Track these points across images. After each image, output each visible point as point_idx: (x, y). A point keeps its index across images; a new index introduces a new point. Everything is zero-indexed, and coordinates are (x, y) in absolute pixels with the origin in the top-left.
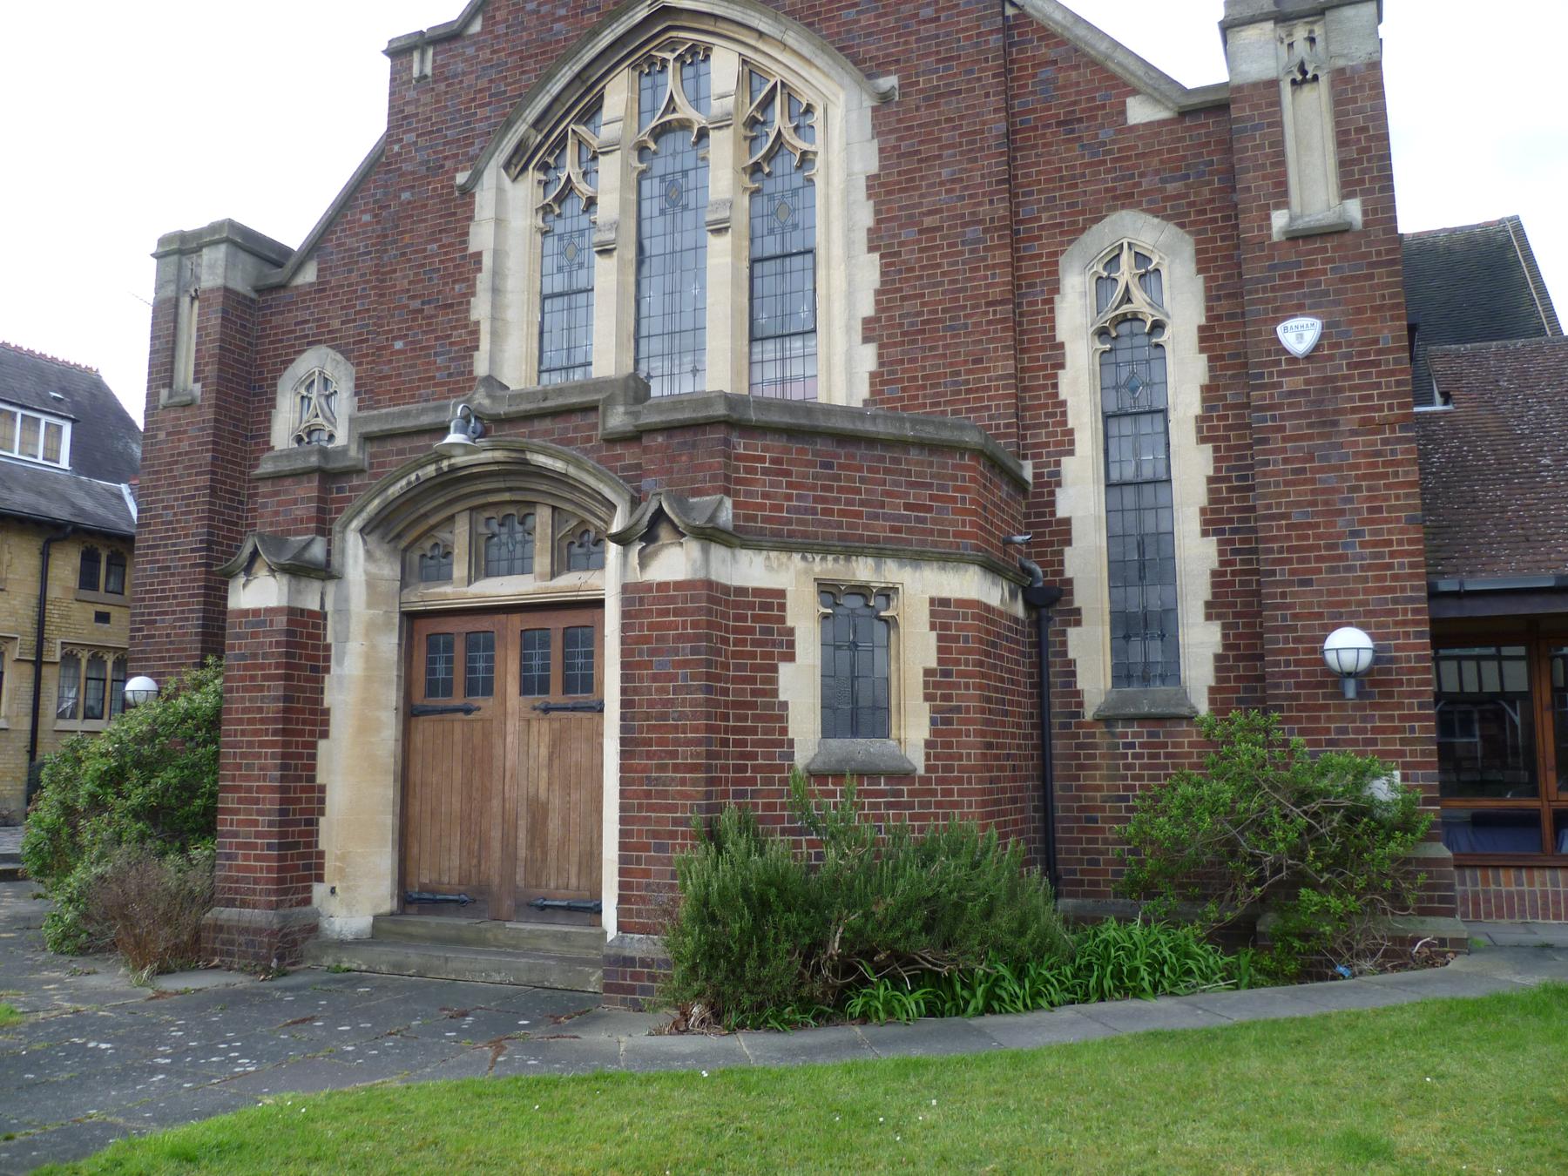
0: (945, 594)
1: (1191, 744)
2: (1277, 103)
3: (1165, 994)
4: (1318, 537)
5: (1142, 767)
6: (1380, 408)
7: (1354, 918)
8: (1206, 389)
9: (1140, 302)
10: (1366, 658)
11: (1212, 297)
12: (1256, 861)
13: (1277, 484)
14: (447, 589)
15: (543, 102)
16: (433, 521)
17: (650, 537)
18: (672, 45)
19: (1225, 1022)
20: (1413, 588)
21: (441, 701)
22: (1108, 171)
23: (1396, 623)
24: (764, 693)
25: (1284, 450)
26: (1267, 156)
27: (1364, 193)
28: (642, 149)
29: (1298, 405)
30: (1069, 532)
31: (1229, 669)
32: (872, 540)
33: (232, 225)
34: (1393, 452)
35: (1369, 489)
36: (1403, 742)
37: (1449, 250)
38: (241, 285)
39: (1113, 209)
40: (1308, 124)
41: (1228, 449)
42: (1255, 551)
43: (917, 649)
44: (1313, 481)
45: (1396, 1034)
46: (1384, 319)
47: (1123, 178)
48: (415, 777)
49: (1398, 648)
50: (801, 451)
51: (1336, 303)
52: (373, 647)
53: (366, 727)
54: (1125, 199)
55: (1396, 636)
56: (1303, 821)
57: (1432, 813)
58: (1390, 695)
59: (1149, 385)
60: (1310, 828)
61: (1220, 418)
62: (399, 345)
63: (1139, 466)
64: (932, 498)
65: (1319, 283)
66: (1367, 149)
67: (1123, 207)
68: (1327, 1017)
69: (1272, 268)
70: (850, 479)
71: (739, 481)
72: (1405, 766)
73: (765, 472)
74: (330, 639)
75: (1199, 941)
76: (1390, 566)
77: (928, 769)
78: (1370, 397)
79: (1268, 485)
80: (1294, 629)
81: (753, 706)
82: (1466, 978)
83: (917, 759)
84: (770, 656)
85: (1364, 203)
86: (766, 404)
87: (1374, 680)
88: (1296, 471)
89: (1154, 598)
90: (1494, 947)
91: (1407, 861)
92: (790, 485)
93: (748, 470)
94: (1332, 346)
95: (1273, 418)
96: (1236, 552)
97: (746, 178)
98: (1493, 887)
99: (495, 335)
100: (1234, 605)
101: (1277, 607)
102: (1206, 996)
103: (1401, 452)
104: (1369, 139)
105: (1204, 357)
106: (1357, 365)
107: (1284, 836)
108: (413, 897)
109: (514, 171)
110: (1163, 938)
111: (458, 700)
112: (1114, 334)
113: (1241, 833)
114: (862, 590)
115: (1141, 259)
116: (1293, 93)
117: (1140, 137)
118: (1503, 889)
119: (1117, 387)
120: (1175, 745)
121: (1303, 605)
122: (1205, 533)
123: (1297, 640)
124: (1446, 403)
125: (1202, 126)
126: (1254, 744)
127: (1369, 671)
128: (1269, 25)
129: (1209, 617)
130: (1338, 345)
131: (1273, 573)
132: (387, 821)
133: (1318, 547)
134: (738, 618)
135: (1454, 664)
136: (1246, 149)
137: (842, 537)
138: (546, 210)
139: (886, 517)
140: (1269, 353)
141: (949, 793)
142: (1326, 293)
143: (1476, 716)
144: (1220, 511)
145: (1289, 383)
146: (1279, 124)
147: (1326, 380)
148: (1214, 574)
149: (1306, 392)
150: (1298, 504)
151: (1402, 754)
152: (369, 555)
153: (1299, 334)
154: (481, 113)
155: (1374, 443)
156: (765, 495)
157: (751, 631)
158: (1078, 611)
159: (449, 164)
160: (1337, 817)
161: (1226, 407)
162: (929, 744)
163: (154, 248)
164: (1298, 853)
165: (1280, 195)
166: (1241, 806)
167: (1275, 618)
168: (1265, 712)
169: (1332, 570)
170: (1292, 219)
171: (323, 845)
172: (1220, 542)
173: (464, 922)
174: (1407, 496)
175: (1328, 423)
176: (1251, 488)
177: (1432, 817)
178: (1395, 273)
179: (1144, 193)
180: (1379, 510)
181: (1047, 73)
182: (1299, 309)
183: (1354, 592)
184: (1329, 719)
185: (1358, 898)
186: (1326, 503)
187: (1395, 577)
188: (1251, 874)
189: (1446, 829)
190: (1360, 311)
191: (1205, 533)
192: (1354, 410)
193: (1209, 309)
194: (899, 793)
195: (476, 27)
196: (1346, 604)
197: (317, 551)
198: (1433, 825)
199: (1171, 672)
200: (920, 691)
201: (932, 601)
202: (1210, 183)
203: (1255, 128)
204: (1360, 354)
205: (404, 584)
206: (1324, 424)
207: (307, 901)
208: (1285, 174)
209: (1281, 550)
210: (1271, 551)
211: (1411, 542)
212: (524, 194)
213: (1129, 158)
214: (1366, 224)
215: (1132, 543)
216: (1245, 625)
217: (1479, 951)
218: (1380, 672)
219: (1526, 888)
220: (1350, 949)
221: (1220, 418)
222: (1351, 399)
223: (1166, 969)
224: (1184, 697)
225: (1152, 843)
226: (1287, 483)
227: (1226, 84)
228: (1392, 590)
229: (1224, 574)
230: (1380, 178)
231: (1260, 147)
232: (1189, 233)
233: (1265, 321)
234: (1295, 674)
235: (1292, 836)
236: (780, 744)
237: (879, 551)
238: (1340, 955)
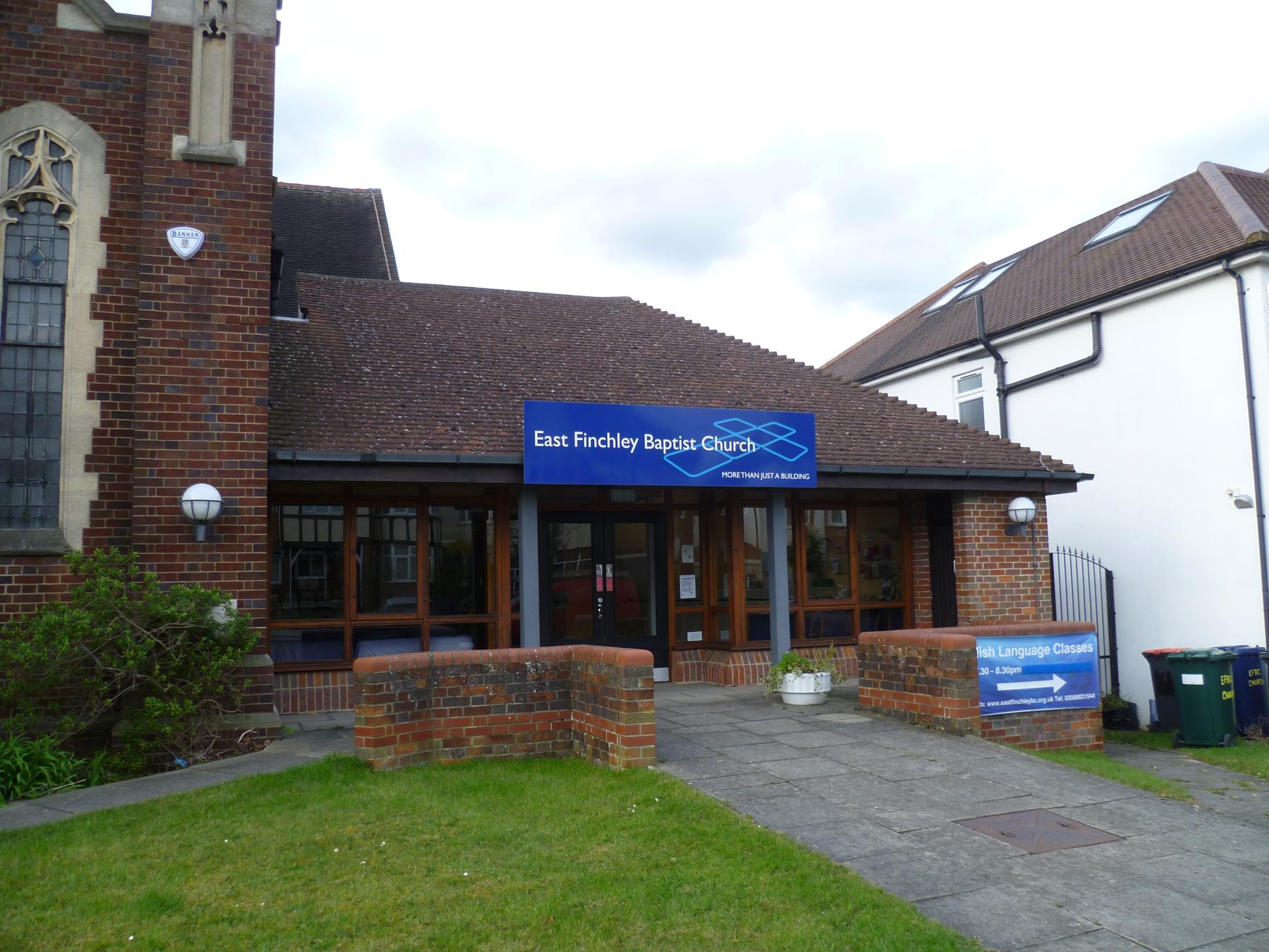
1: (64, 579)
2: (189, 47)
3: (16, 799)
4: (185, 408)
5: (17, 599)
6: (244, 311)
7: (192, 719)
8: (102, 273)
9: (50, 185)
10: (215, 509)
11: (116, 195)
12: (109, 677)
13: (155, 361)
19: (67, 816)
20: (257, 456)
22: (32, 63)
23: (242, 483)
25: (163, 334)
26: (175, 88)
27: (250, 138)
29: (179, 298)
31: (103, 514)
34: (251, 347)
35: (230, 374)
36: (241, 576)
37: (329, 205)
40: (212, 71)
41: (117, 327)
42: (131, 416)
44: (185, 362)
45: (210, 807)
46: (253, 241)
47: (46, 73)
49: (242, 502)
51: (217, 221)
54: (48, 93)
55: (241, 492)
56: (152, 642)
57: (259, 632)
58: (233, 539)
59: (52, 260)
60: (158, 646)
61: (112, 299)
63: (34, 332)
65: (206, 202)
66: (257, 104)
67: (44, 98)
68: (157, 801)
69: (168, 181)
72: (242, 595)
75: (53, 749)
76: (241, 437)
78: (237, 301)
79: (147, 361)
80: (159, 482)
82: (276, 757)
85: (248, 146)
87: (220, 527)
88: (171, 353)
89: (39, 450)
90: (303, 732)
91: (238, 670)
94: (211, 255)
95: (157, 306)
96: (116, 415)
98: (307, 687)
100: (111, 460)
101: (147, 464)
102: (59, 795)
103: (257, 348)
104: (258, 96)
105: (104, 245)
106: (230, 274)
107: (134, 654)
110: (18, 750)
112: (22, 210)
113: (97, 654)
115: (55, 148)
116: (204, 43)
117: (68, 41)
118: (315, 688)
119: (20, 258)
120: (49, 579)
121: (168, 464)
122: (90, 397)
123: (160, 492)
124: (304, 317)
125: (123, 47)
126: (113, 577)
127: (217, 519)
129: (88, 469)
130: (215, 255)
131: (145, 435)
133: (185, 417)
135: (311, 522)
136: (158, 78)
140: (158, 251)
142: (210, 211)
143: (325, 559)
144: (105, 379)
145: (173, 279)
146: (189, 65)
147: (203, 281)
148: (96, 432)
149: (186, 289)
150: (171, 380)
151: (239, 586)
153: (185, 240)
155: (236, 338)
160: (180, 637)
161: (119, 291)
164: (146, 668)
165: (183, 125)
166: (97, 631)
167: (143, 472)
168: (123, 551)
169: (195, 436)
170: (189, 144)
172: (103, 405)
174: (259, 383)
175: (202, 317)
176: (133, 362)
177: (259, 634)
178: (266, 207)
180: (235, 391)
182: (186, 220)
183: (210, 456)
184: (183, 558)
185: (195, 702)
186: (194, 381)
187: (244, 446)
188: (105, 687)
189: (271, 644)
191: (90, 397)
192: (224, 310)
193: (112, 205)
196: (204, 464)
198: (260, 641)
199: (50, 515)
202: (126, 98)
203: (168, 62)
204: (233, 265)
206: (197, 317)
208: (188, 106)
209: (153, 417)
210: (145, 416)
211: (258, 419)
213: (54, 56)
214: (248, 163)
215: (22, 398)
216: (120, 478)
217: (291, 736)
218: (227, 520)
219: (331, 686)
220: (188, 744)
221: (112, 299)
222: (222, 300)
223: (19, 776)
224: (60, 538)
225: (13, 666)
226: (163, 362)
227: (147, 18)
229: (104, 433)
230: (263, 130)
232: (102, 135)
233: (158, 224)
234: (157, 520)
235: (142, 654)
238: (179, 750)
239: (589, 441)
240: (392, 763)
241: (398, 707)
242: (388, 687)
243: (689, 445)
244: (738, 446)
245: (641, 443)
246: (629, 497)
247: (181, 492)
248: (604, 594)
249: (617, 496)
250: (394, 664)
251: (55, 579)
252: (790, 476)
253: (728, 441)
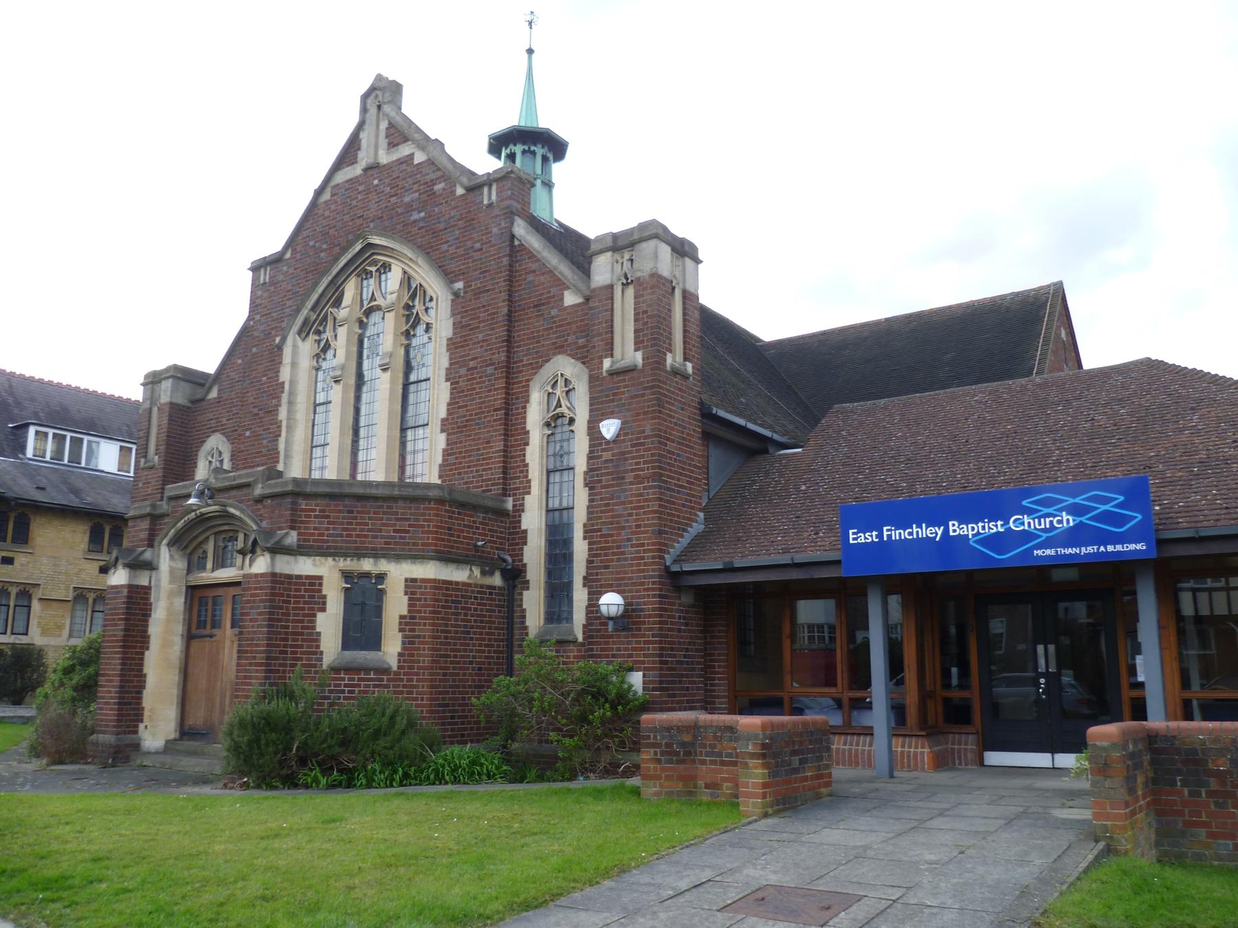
0: (414, 576)
14: (204, 575)
15: (315, 297)
16: (200, 539)
17: (253, 552)
18: (375, 263)
21: (202, 632)
24: (308, 628)
28: (361, 323)
30: (526, 538)
32: (373, 549)
33: (176, 368)
37: (1008, 310)
38: (181, 400)
39: (555, 354)
43: (396, 605)
44: (612, 510)
48: (190, 671)
50: (336, 505)
51: (629, 410)
52: (171, 604)
53: (166, 644)
54: (560, 349)
62: (248, 434)
64: (410, 526)
67: (559, 353)
70: (362, 518)
71: (302, 522)
72: (645, 669)
73: (316, 517)
74: (152, 600)
77: (399, 667)
81: (302, 634)
83: (393, 663)
84: (313, 609)
86: (317, 482)
92: (329, 523)
93: (307, 516)
97: (403, 338)
99: (289, 427)
103: (651, 494)
108: (186, 732)
109: (304, 335)
111: (208, 631)
114: (367, 575)
115: (567, 382)
119: (555, 455)
128: (609, 254)
132: (174, 693)
134: (297, 590)
137: (357, 548)
138: (317, 356)
139: (382, 537)
141: (411, 680)
142: (624, 405)
150: (605, 523)
152: (172, 557)
154: (289, 303)
156: (315, 529)
157: (303, 596)
158: (528, 582)
159: (273, 332)
162: (400, 655)
163: (142, 380)
169: (618, 560)
170: (613, 363)
171: (144, 705)
173: (197, 743)
179: (568, 345)
181: (530, 278)
184: (614, 643)
187: (645, 564)
190: (638, 414)
192: (632, 470)
194: (382, 680)
195: (288, 255)
197: (148, 555)
200: (397, 627)
201: (406, 580)
205: (189, 571)
206: (618, 478)
207: (136, 732)
212: (307, 348)
224: (571, 631)
228: (643, 571)
231: (600, 323)
236: (316, 653)
237: (376, 555)
239: (896, 535)
240: (657, 794)
241: (663, 753)
242: (655, 737)
243: (997, 527)
244: (1051, 522)
245: (946, 530)
246: (1072, 574)
247: (598, 600)
248: (1046, 674)
249: (1057, 575)
250: (660, 721)
251: (568, 657)
252: (1119, 548)
253: (1039, 518)
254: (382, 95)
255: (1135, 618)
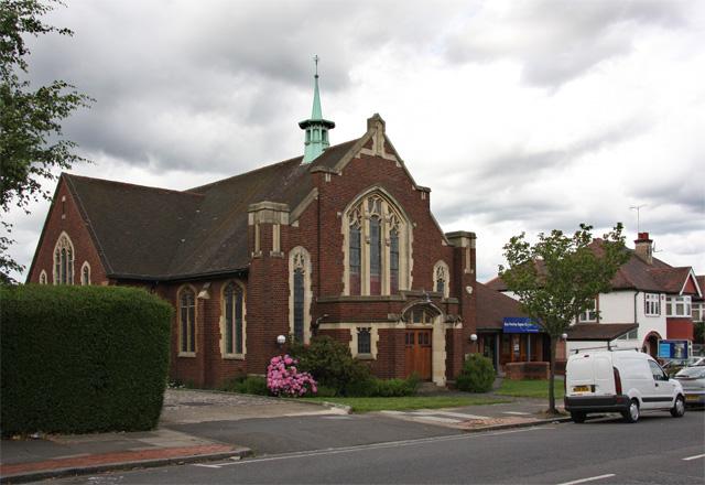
43: (375, 337)
254: (376, 123)
255: (312, 305)
